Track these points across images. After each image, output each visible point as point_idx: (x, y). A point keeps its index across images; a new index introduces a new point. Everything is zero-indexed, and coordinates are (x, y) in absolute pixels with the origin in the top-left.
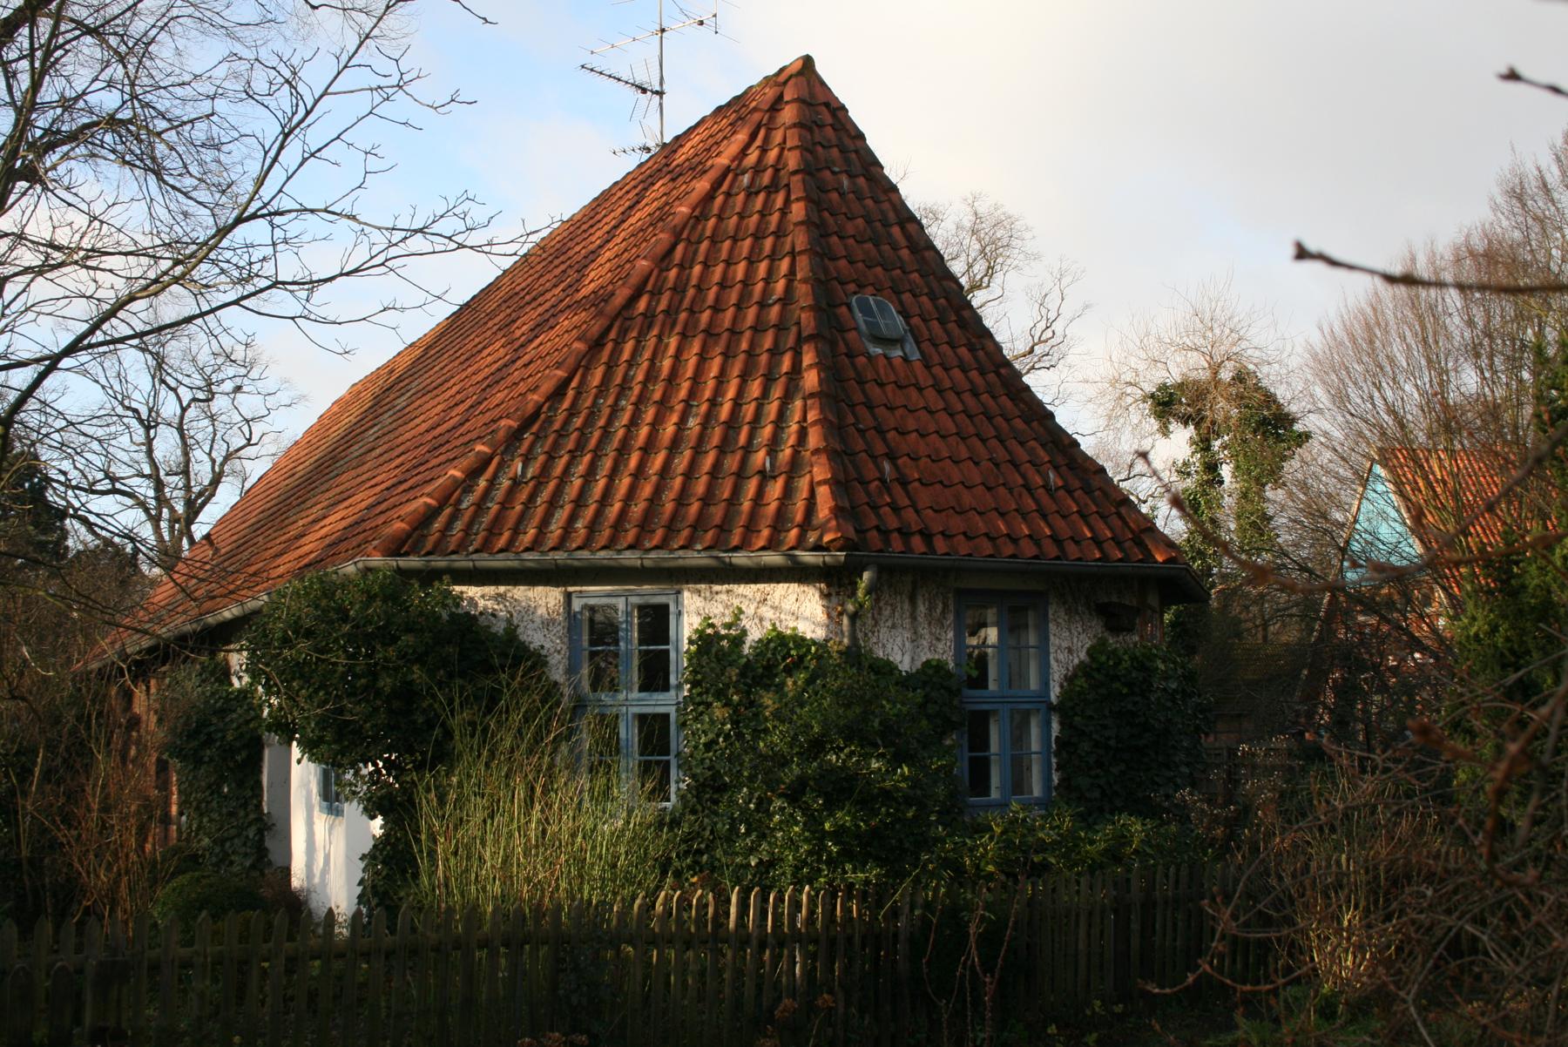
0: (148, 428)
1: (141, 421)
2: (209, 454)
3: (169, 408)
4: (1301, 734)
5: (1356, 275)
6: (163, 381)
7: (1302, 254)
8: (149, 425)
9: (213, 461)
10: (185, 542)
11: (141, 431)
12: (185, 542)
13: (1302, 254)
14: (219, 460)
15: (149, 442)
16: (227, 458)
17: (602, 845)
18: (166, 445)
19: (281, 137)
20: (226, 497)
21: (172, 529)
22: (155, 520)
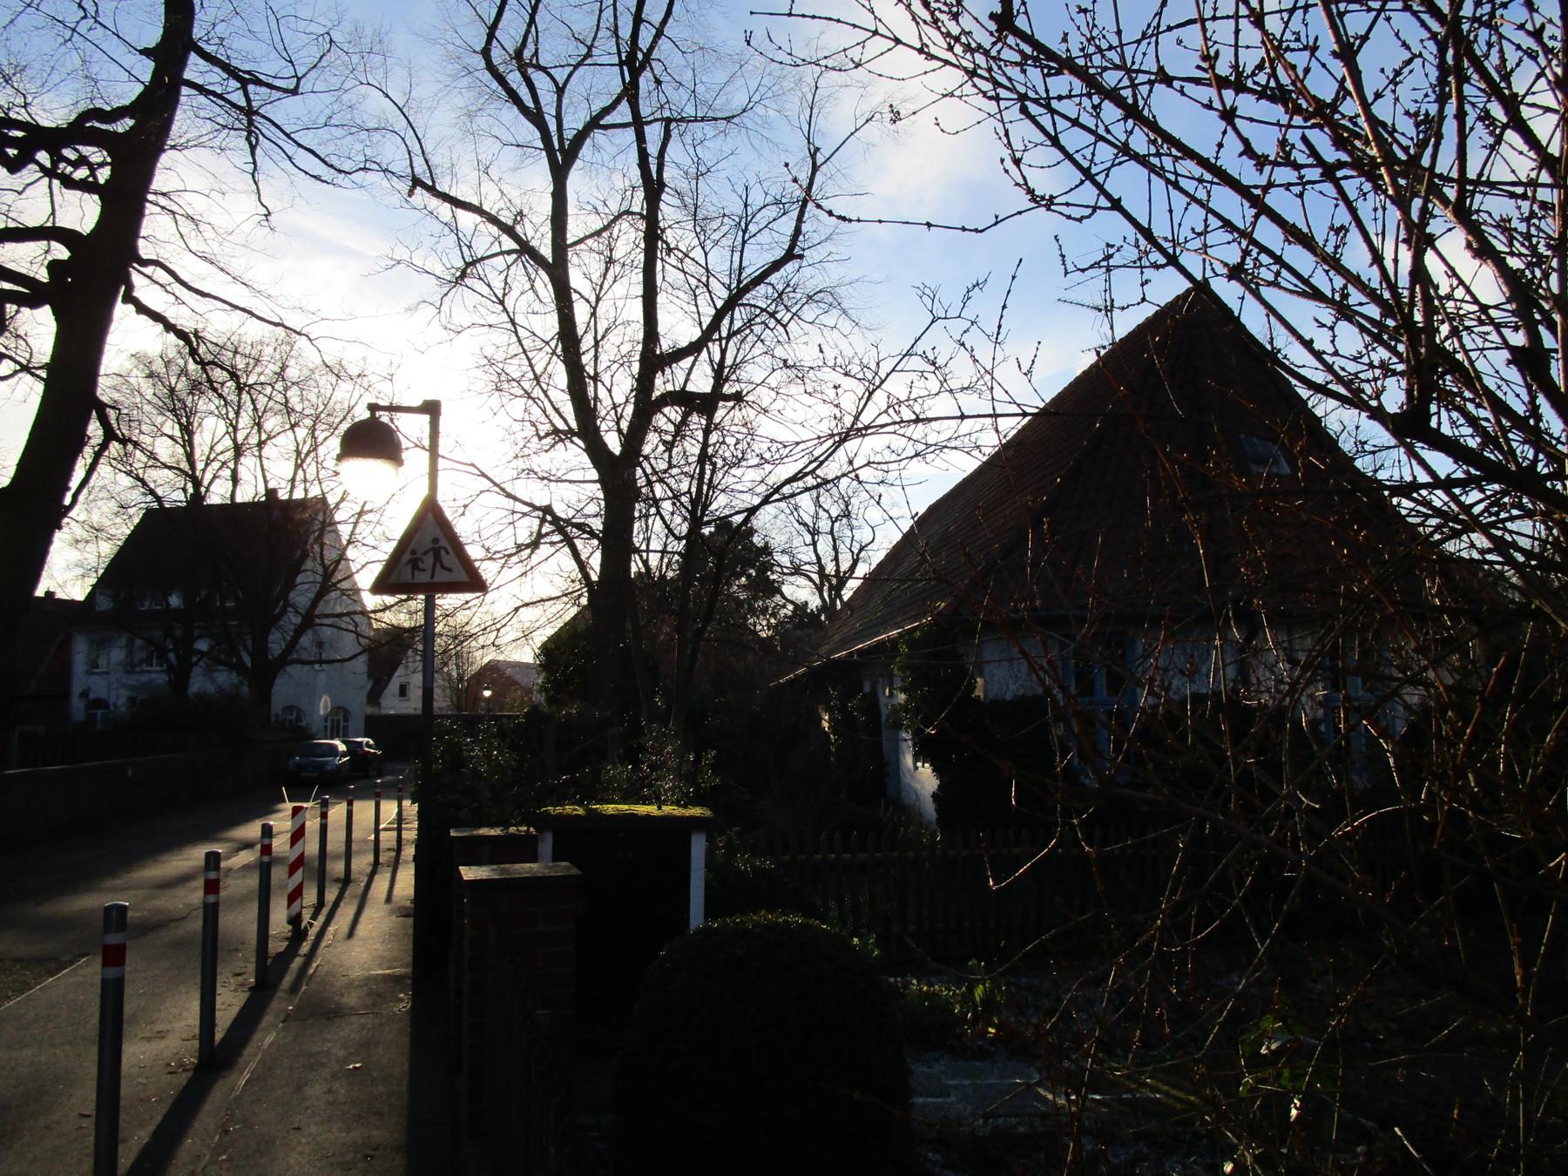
0: (813, 535)
1: (809, 531)
2: (850, 549)
3: (824, 525)
4: (1174, 316)
5: (1024, 174)
6: (820, 506)
7: (752, 13)
8: (814, 532)
9: (853, 553)
10: (838, 602)
11: (810, 537)
12: (838, 602)
13: (752, 13)
14: (856, 551)
15: (814, 544)
16: (861, 549)
17: (1167, 1094)
18: (824, 545)
19: (867, 394)
20: (853, 585)
21: (830, 596)
22: (820, 589)
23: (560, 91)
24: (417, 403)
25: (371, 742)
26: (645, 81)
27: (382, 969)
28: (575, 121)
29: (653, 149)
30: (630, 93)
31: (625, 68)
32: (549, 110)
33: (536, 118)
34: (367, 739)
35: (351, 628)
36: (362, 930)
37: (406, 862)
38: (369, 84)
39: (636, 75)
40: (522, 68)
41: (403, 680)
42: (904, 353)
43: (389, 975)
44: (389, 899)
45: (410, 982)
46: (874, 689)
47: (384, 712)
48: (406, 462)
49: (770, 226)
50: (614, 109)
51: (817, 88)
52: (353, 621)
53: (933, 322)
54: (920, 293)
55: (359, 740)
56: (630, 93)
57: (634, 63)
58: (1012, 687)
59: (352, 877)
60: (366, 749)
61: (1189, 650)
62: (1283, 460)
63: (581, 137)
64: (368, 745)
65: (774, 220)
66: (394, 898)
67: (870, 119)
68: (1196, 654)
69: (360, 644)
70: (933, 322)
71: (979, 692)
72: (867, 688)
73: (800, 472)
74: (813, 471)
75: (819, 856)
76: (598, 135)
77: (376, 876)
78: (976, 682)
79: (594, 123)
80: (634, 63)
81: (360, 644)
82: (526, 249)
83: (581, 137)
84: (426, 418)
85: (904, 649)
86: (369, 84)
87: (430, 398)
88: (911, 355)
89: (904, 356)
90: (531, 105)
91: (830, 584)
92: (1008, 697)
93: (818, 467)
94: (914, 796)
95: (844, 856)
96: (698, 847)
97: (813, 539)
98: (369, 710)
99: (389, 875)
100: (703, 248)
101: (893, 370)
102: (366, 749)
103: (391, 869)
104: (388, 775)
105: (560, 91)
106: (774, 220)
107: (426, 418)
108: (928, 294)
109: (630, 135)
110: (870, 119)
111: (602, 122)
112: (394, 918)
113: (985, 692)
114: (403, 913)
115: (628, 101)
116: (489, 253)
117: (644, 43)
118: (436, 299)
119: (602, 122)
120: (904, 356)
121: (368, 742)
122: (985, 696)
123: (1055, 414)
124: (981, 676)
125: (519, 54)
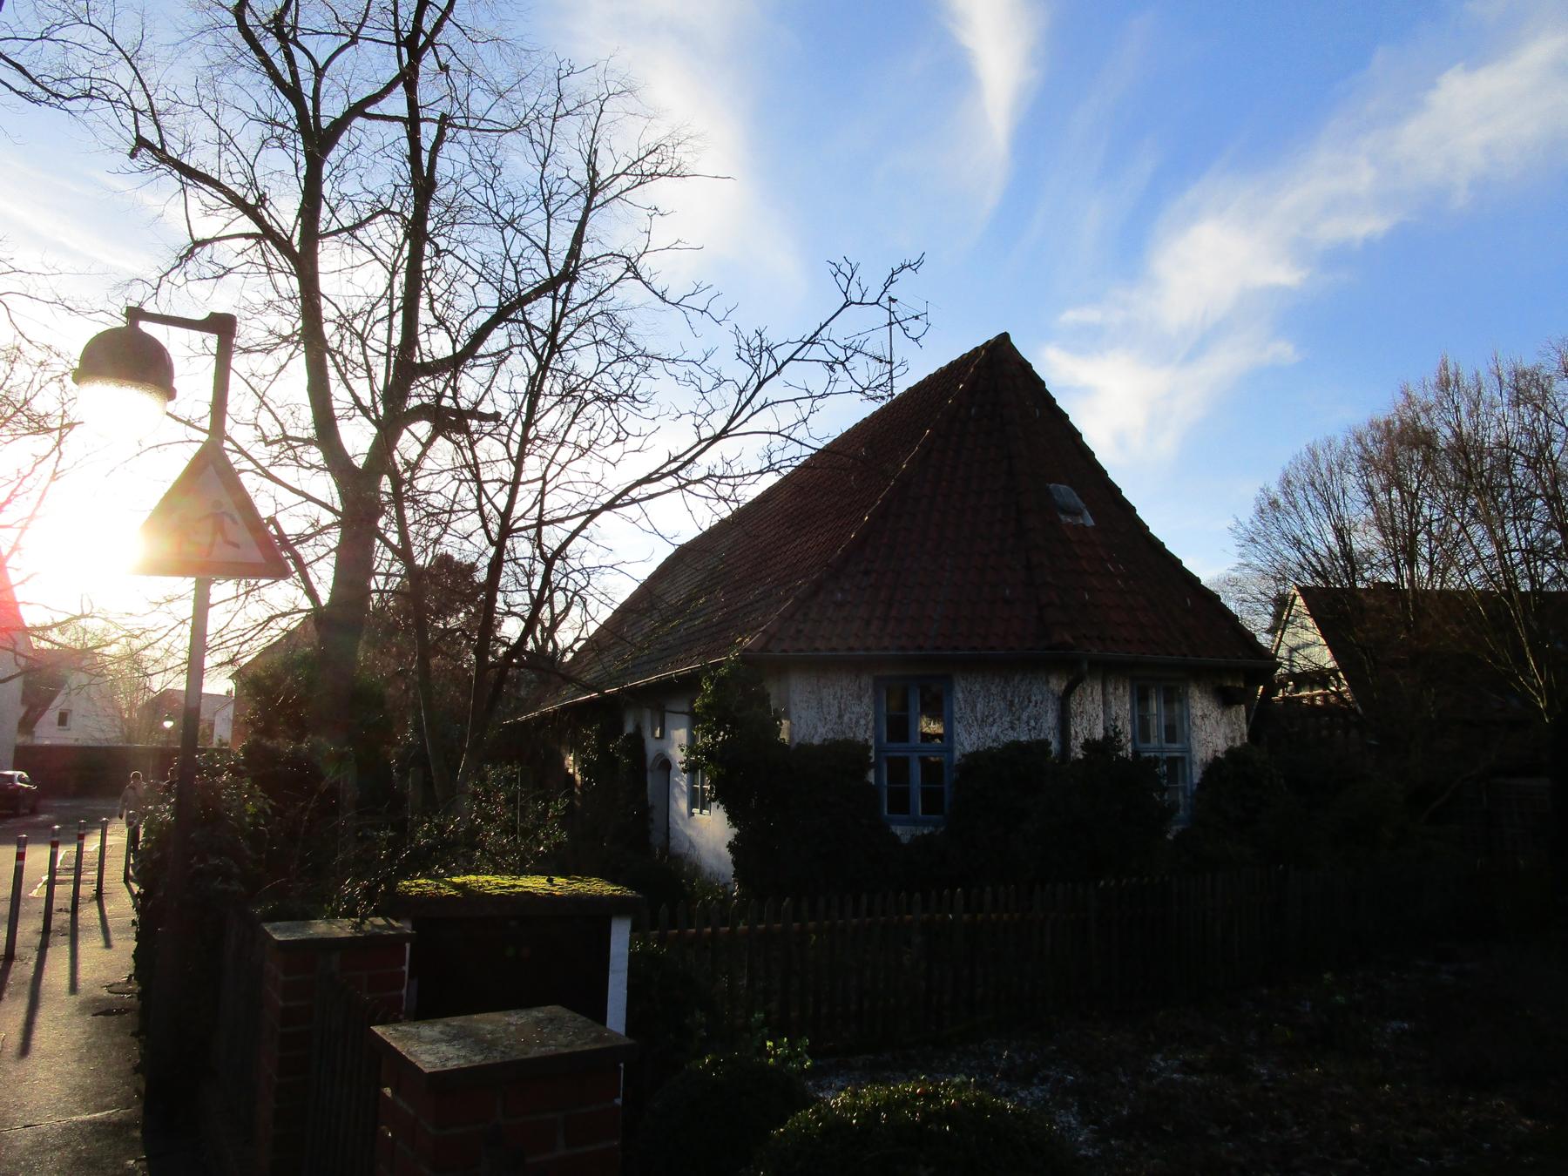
21: (542, 635)
23: (319, 73)
24: (201, 315)
25: (25, 775)
26: (428, 62)
27: (88, 1110)
28: (332, 109)
29: (427, 144)
30: (408, 78)
31: (404, 50)
32: (307, 88)
33: (293, 93)
34: (19, 773)
35: (8, 645)
36: (43, 1036)
37: (88, 929)
38: (91, 24)
39: (416, 55)
40: (281, 36)
41: (64, 707)
42: (805, 340)
43: (102, 1123)
44: (73, 988)
45: (137, 1134)
46: (639, 729)
47: (38, 742)
48: (179, 395)
49: (623, 196)
50: (383, 98)
51: (602, 111)
52: (11, 637)
53: (845, 306)
54: (835, 270)
55: (10, 773)
56: (408, 78)
57: (413, 45)
58: (822, 730)
59: (17, 951)
60: (19, 784)
61: (1009, 695)
62: (1087, 512)
63: (341, 125)
64: (21, 779)
65: (628, 189)
66: (81, 985)
67: (654, 151)
68: (1016, 700)
69: (17, 664)
70: (845, 306)
71: (784, 735)
72: (629, 728)
73: (656, 472)
74: (675, 471)
75: (693, 930)
76: (358, 122)
77: (49, 950)
78: (781, 724)
79: (358, 110)
80: (413, 45)
81: (17, 664)
82: (267, 233)
83: (341, 125)
84: (212, 340)
85: (707, 686)
86: (91, 24)
87: (220, 309)
88: (813, 343)
89: (806, 344)
90: (288, 78)
91: (543, 626)
92: (816, 741)
93: (681, 468)
94: (687, 845)
95: (722, 929)
96: (620, 938)
97: (529, 580)
98: (21, 740)
99: (67, 948)
100: (546, 207)
101: (791, 358)
102: (19, 784)
103: (67, 939)
104: (44, 813)
105: (319, 73)
106: (628, 189)
107: (212, 340)
108: (845, 273)
109: (399, 130)
110: (654, 151)
111: (368, 110)
112: (89, 1017)
113: (791, 735)
114: (102, 1010)
115: (404, 86)
116: (220, 235)
117: (427, 26)
118: (153, 277)
119: (368, 110)
120: (806, 344)
121: (20, 776)
122: (791, 739)
123: (815, 468)
124: (788, 718)
125: (278, 19)
